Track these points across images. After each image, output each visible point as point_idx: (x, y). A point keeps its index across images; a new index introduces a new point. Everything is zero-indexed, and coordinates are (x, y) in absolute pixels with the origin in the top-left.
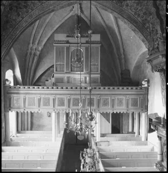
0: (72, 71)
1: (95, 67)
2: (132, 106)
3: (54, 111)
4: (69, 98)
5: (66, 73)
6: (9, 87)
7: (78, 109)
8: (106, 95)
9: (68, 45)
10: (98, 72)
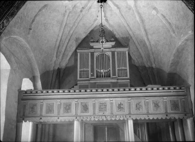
0: (98, 77)
1: (126, 71)
2: (172, 110)
3: (76, 119)
6: (25, 93)
8: (138, 97)
10: (126, 77)
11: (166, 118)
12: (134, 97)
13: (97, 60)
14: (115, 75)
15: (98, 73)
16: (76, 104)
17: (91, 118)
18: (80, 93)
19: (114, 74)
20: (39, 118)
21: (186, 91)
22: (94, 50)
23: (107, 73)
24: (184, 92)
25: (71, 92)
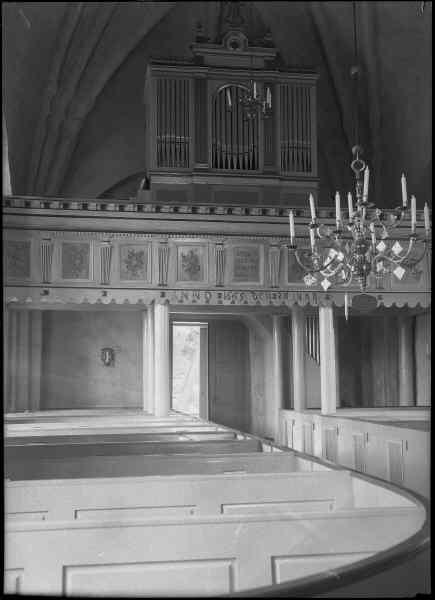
3: (163, 300)
7: (252, 292)
9: (201, 72)
12: (250, 236)
14: (273, 164)
16: (160, 251)
18: (174, 216)
19: (270, 160)
20: (42, 290)
23: (246, 157)
25: (89, 208)
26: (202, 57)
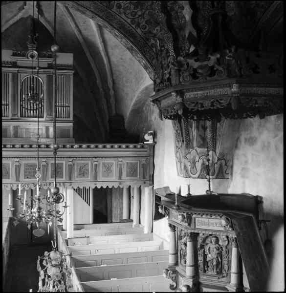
4: (17, 164)
5: (12, 119)
7: (33, 183)
9: (15, 70)
10: (68, 119)
11: (119, 186)
13: (22, 86)
15: (24, 109)
17: (12, 186)
21: (148, 151)
22: (17, 69)
24: (146, 151)
26: (16, 62)
